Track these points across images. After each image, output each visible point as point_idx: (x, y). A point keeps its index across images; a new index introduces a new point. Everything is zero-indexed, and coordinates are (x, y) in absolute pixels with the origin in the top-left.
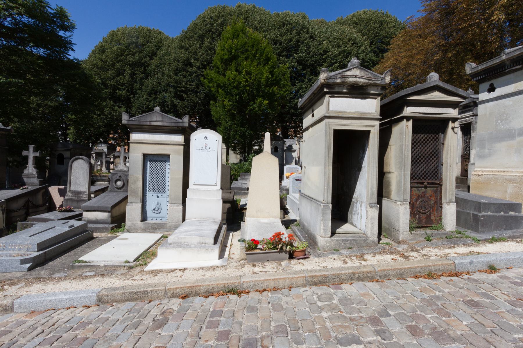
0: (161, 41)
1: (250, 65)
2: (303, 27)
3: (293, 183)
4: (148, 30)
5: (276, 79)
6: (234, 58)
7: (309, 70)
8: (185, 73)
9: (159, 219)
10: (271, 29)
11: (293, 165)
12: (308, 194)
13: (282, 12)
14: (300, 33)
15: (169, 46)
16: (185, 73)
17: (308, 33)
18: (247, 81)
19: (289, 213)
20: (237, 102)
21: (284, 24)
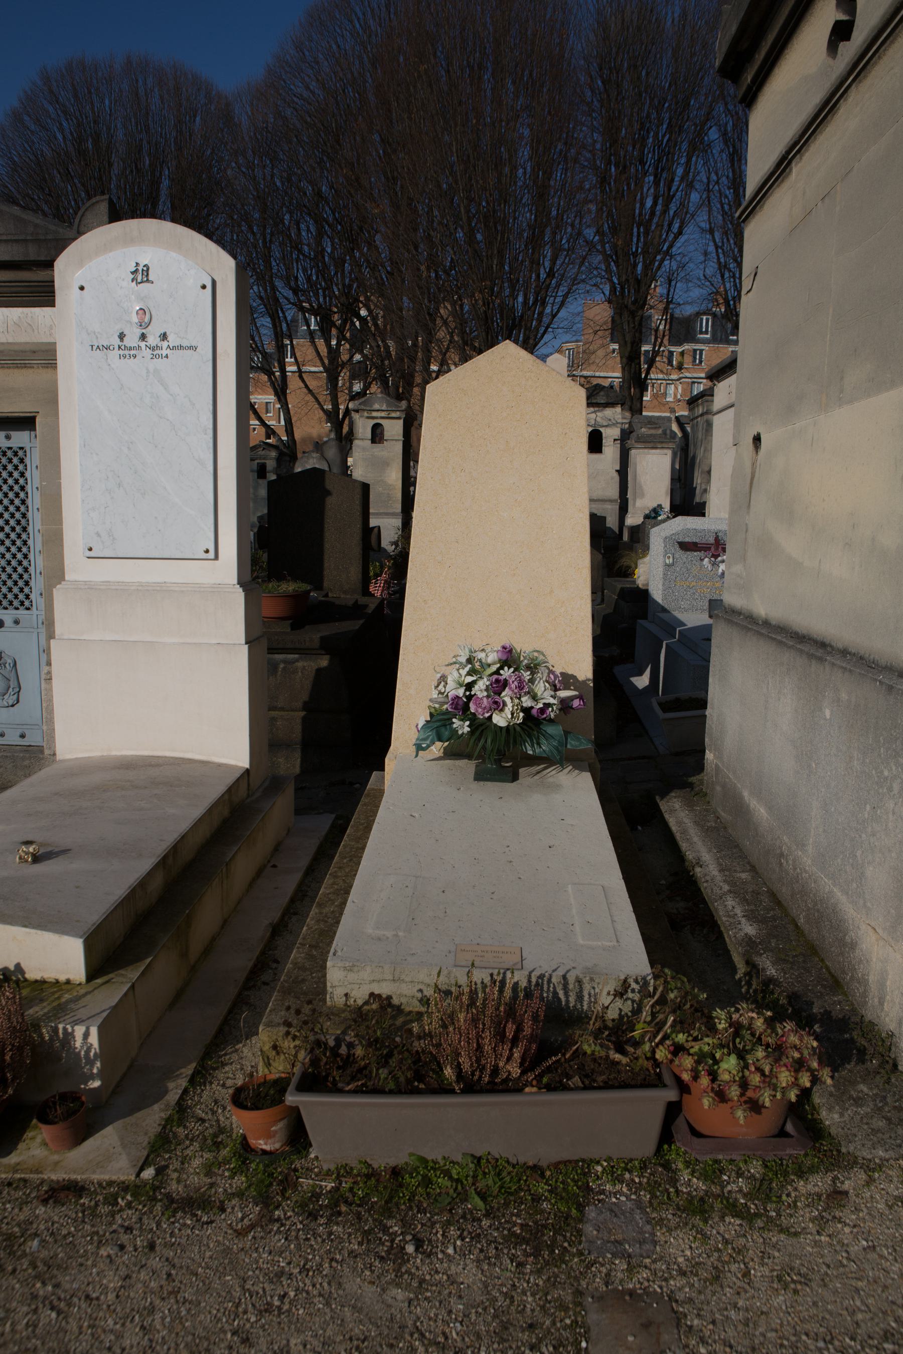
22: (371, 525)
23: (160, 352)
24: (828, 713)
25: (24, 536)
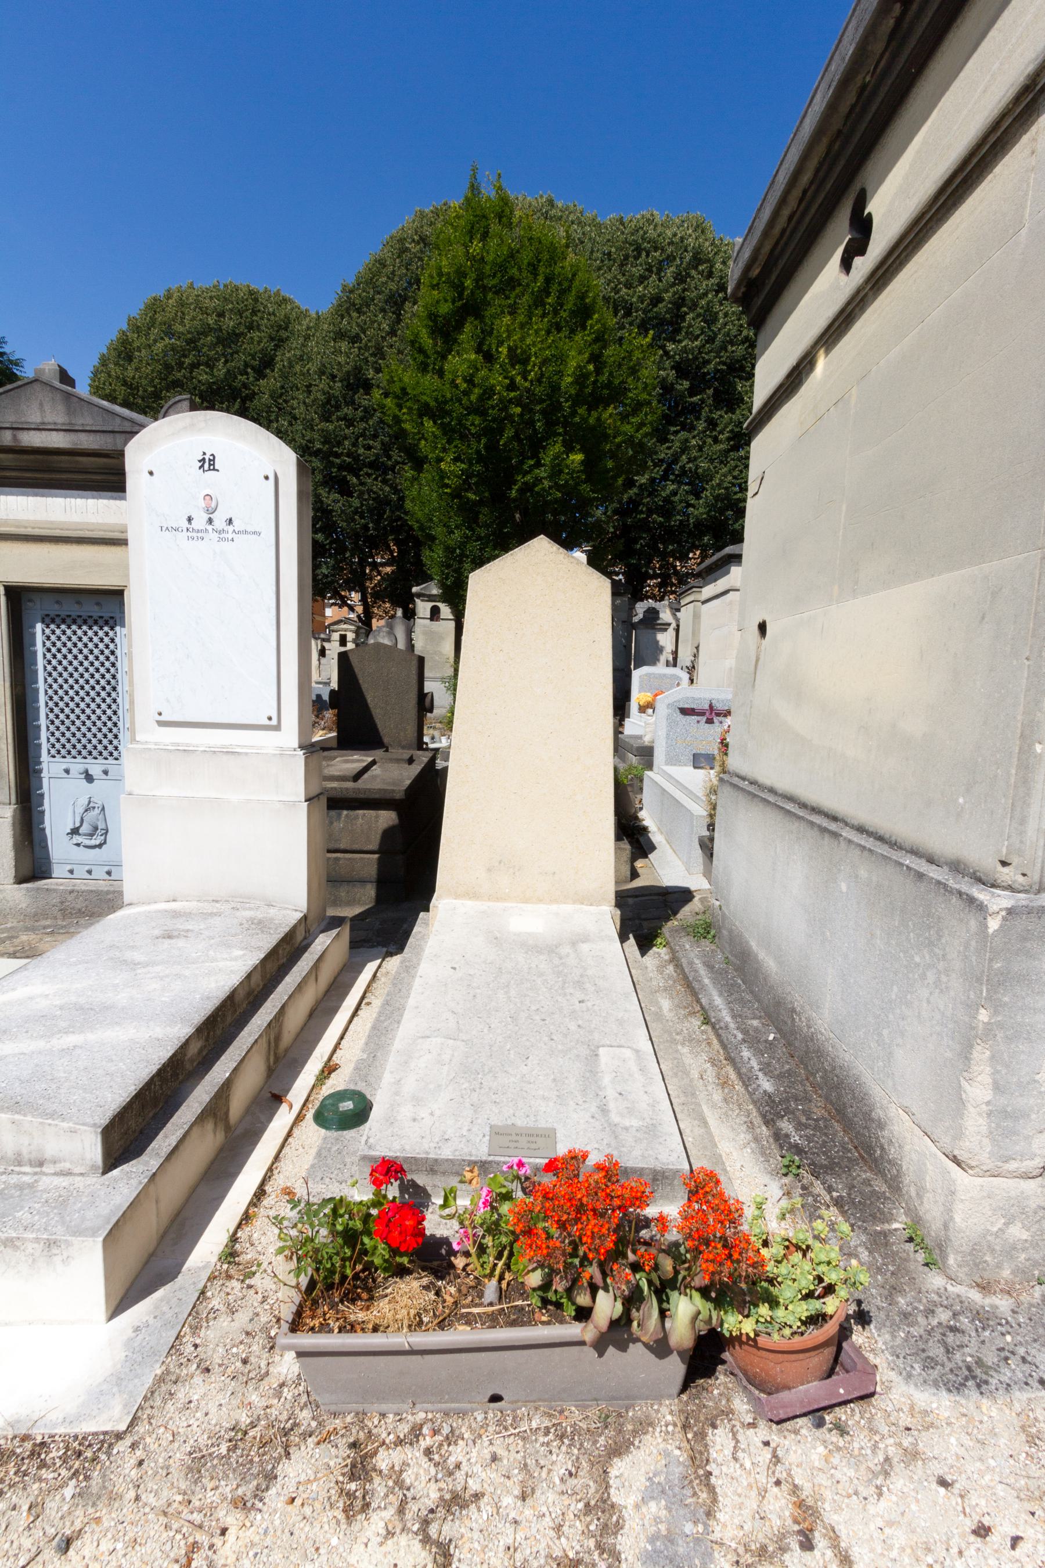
0: (285, 325)
1: (522, 326)
2: (698, 259)
3: (671, 724)
4: (251, 293)
5: (610, 382)
6: (470, 309)
7: (710, 392)
8: (348, 411)
9: (99, 873)
10: (599, 269)
11: (660, 669)
12: (783, 784)
13: (635, 216)
14: (688, 275)
15: (307, 338)
16: (348, 411)
17: (710, 275)
18: (512, 386)
19: (653, 848)
20: (480, 459)
21: (639, 250)
22: (426, 691)
23: (226, 536)
24: (844, 887)
25: (114, 695)
